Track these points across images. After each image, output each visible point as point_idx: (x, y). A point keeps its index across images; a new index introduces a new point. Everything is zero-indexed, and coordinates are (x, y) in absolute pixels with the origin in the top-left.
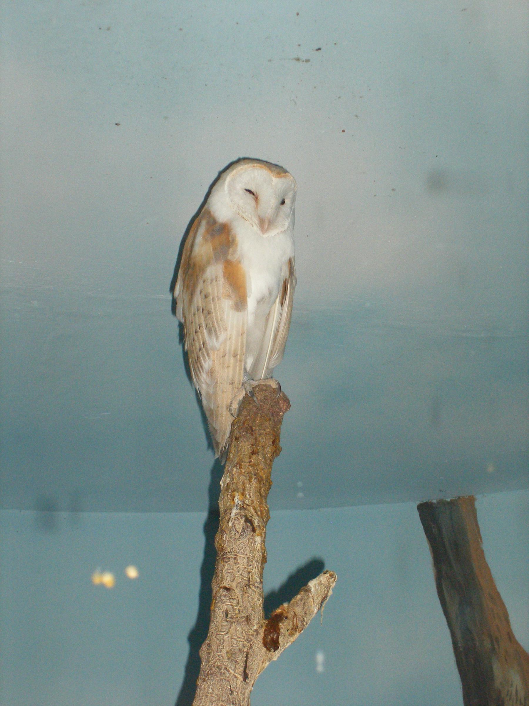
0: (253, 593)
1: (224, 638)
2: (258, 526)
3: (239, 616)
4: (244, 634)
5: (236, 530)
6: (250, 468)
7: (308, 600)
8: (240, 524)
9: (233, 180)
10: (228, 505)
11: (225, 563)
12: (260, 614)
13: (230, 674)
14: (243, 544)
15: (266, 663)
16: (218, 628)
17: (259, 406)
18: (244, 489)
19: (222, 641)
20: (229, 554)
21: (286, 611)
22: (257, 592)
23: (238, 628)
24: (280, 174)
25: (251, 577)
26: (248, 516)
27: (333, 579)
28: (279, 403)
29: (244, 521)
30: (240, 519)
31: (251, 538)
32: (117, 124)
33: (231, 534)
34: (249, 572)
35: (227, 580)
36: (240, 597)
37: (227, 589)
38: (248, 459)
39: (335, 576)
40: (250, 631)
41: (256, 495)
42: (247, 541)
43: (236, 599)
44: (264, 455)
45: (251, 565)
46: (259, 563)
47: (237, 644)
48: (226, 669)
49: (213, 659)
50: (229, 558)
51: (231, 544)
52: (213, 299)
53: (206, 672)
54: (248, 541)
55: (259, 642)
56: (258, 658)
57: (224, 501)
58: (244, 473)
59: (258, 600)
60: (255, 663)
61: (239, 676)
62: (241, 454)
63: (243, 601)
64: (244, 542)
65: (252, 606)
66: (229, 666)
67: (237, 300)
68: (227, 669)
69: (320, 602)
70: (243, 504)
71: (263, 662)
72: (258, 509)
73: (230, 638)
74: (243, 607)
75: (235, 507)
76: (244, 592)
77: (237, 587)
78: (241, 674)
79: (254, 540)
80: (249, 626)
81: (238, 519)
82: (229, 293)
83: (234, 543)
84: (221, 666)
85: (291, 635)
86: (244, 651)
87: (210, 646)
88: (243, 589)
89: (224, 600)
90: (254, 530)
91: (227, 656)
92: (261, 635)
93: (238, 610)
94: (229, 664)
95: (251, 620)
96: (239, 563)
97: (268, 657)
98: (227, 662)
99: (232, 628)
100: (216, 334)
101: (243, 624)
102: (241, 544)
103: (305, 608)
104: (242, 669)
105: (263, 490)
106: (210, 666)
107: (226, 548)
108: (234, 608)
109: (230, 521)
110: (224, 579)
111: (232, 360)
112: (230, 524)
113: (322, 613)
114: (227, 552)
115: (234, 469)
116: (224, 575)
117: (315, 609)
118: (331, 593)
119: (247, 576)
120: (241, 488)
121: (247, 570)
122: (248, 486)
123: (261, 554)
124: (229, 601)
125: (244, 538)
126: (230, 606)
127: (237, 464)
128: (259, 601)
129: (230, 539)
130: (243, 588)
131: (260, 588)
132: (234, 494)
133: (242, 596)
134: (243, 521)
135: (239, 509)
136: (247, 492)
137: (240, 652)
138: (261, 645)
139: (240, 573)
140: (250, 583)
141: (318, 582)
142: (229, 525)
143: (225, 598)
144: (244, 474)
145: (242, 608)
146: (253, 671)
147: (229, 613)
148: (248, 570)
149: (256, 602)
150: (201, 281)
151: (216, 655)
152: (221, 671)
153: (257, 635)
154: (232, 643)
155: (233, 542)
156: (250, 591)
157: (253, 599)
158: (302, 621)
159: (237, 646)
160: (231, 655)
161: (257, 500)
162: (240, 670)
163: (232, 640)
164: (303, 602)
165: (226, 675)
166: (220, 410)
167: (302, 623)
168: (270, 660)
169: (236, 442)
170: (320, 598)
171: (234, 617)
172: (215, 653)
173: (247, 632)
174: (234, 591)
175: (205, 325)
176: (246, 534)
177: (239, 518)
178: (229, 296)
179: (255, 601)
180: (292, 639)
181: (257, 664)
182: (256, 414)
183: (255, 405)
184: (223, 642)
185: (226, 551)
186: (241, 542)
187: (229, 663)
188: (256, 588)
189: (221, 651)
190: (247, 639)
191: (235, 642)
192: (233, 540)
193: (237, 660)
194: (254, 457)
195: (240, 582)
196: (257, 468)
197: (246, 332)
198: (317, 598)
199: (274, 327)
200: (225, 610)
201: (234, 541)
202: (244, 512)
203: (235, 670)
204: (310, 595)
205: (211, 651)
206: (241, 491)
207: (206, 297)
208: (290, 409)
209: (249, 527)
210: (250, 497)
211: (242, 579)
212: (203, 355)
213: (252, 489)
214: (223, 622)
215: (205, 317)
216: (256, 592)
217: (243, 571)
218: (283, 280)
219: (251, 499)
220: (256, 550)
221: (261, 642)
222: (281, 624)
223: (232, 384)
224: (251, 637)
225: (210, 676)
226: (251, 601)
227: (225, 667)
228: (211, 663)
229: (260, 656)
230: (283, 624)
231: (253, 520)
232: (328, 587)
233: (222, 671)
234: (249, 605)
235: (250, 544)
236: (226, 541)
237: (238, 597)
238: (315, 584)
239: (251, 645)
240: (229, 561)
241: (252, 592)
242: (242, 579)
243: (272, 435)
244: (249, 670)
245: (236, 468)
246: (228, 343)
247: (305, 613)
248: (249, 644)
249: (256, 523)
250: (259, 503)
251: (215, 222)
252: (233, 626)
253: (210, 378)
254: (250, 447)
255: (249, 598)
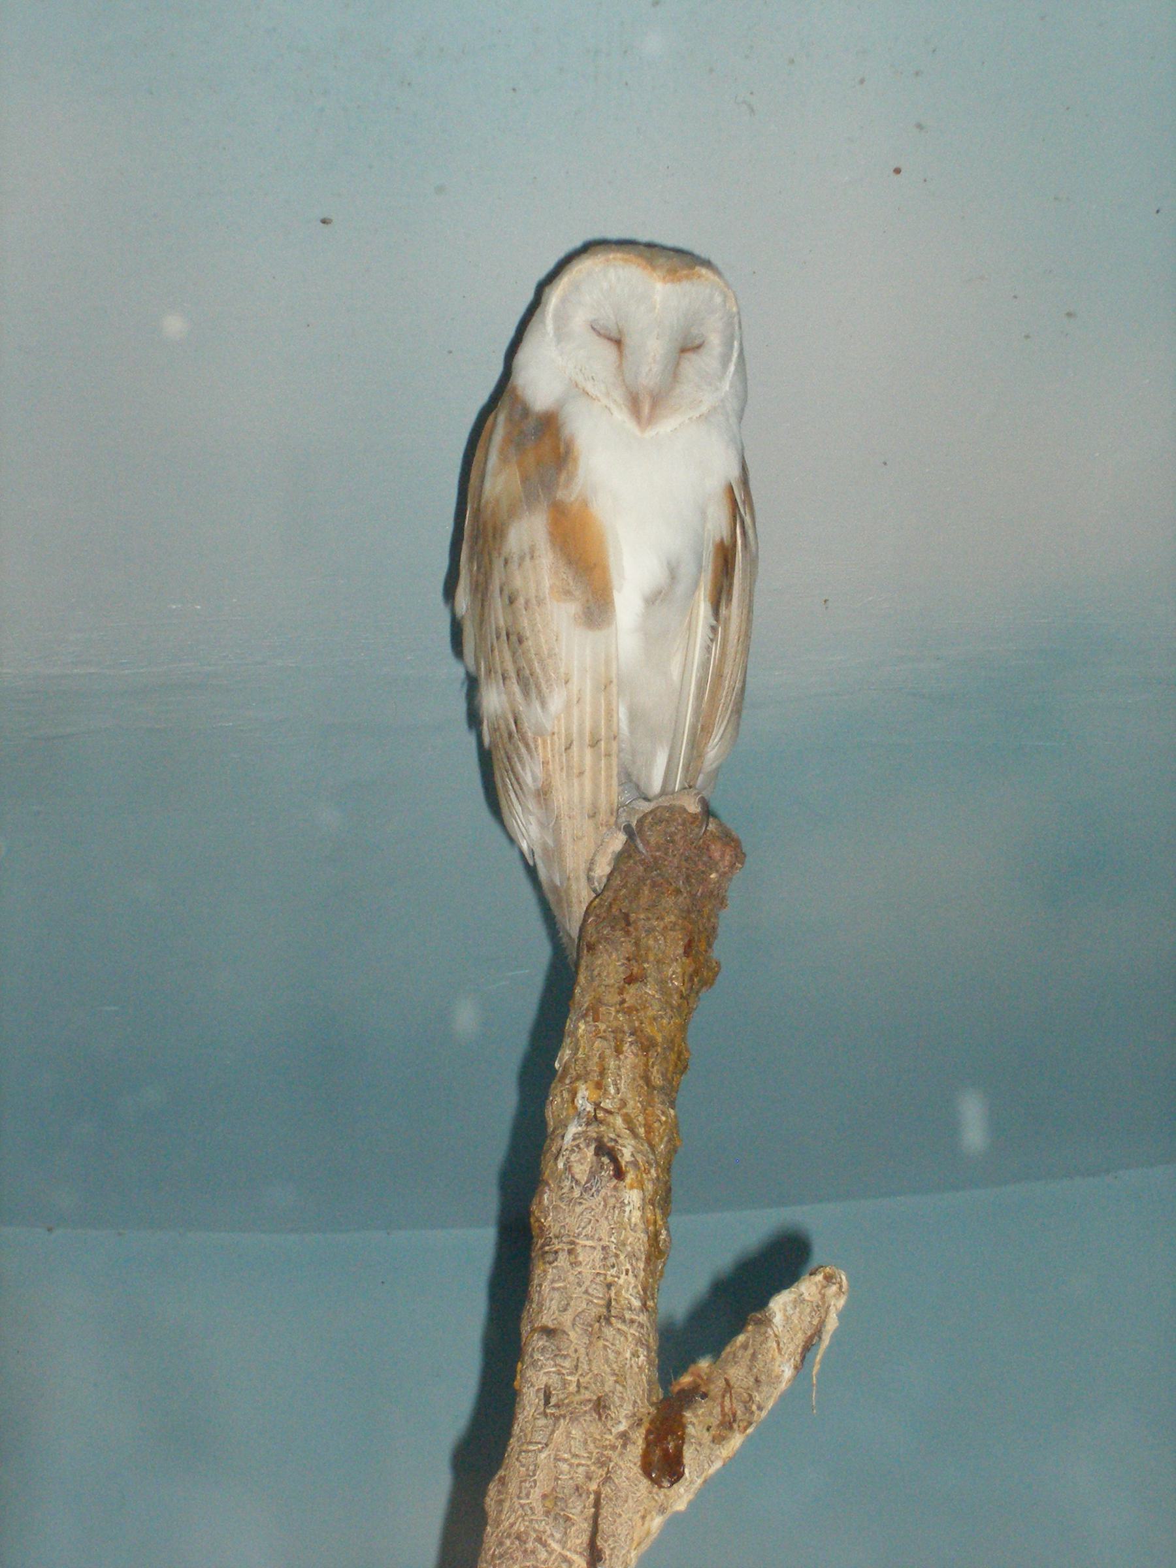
0: (618, 1336)
1: (536, 1459)
2: (632, 1161)
3: (577, 1398)
4: (591, 1446)
5: (573, 1177)
6: (621, 1019)
7: (764, 1346)
8: (583, 1162)
9: (564, 300)
10: (562, 1117)
11: (548, 1266)
12: (641, 1392)
13: (550, 1553)
14: (590, 1213)
15: (652, 1519)
16: (525, 1435)
17: (652, 860)
18: (602, 1073)
19: (531, 1468)
20: (555, 1241)
21: (705, 1378)
22: (631, 1333)
23: (573, 1432)
24: (676, 271)
25: (613, 1295)
26: (606, 1140)
27: (834, 1288)
28: (708, 850)
29: (593, 1152)
30: (585, 1149)
31: (612, 1196)
32: (324, 221)
33: (562, 1188)
34: (609, 1286)
35: (549, 1308)
36: (582, 1351)
37: (549, 1332)
38: (616, 995)
39: (839, 1280)
40: (607, 1436)
41: (636, 1084)
42: (600, 1204)
43: (570, 1357)
44: (662, 983)
45: (613, 1266)
46: (637, 1259)
47: (572, 1473)
48: (539, 1540)
49: (509, 1517)
50: (556, 1252)
51: (561, 1216)
52: (527, 602)
53: (491, 1552)
54: (602, 1203)
55: (632, 1465)
56: (629, 1506)
57: (554, 1108)
58: (604, 1032)
59: (635, 1354)
60: (623, 1522)
61: (575, 1557)
62: (599, 986)
63: (590, 1360)
64: (594, 1207)
65: (616, 1371)
66: (549, 1532)
67: (588, 601)
68: (543, 1539)
69: (800, 1350)
70: (595, 1110)
71: (643, 1517)
72: (638, 1120)
73: (552, 1460)
74: (589, 1376)
75: (576, 1120)
76: (594, 1335)
77: (573, 1325)
78: (581, 1553)
79: (620, 1201)
80: (605, 1425)
81: (580, 1148)
82: (569, 584)
83: (569, 1212)
84: (527, 1534)
85: (718, 1440)
86: (588, 1490)
87: (503, 1484)
88: (590, 1329)
89: (540, 1360)
90: (619, 1174)
91: (544, 1506)
92: (638, 1446)
93: (575, 1384)
94: (547, 1528)
95: (612, 1407)
96: (581, 1263)
97: (656, 1501)
98: (543, 1523)
99: (557, 1432)
100: (539, 691)
101: (585, 1420)
102: (585, 1213)
103: (756, 1367)
104: (585, 1538)
105: (655, 1071)
106: (500, 1534)
107: (550, 1226)
108: (564, 1379)
109: (561, 1157)
110: (544, 1308)
111: (588, 753)
112: (561, 1165)
113: (814, 1379)
114: (553, 1237)
115: (580, 1024)
116: (545, 1296)
117: (787, 1370)
118: (832, 1323)
119: (601, 1296)
120: (595, 1071)
121: (602, 1279)
122: (612, 1064)
123: (642, 1235)
124: (552, 1363)
125: (593, 1196)
126: (554, 1375)
127: (587, 1010)
128: (638, 1357)
129: (559, 1203)
130: (591, 1326)
131: (639, 1323)
132: (576, 1087)
133: (587, 1348)
134: (590, 1152)
135: (584, 1124)
136: (609, 1080)
137: (577, 1494)
138: (636, 1471)
139: (583, 1289)
140: (610, 1311)
141: (793, 1296)
142: (557, 1167)
143: (542, 1356)
144: (604, 1034)
145: (587, 1378)
146: (616, 1542)
147: (553, 1392)
148: (605, 1279)
149: (628, 1362)
150: (498, 564)
151: (517, 1506)
152: (527, 1546)
153: (624, 1446)
154: (557, 1472)
155: (565, 1210)
156: (609, 1332)
157: (618, 1353)
158: (745, 1402)
159: (572, 1478)
160: (553, 1503)
161: (637, 1098)
162: (578, 1541)
163: (559, 1463)
164: (750, 1351)
165: (539, 1557)
166: (574, 887)
167: (745, 1407)
168: (662, 1510)
169: (589, 957)
170: (800, 1339)
171: (563, 1404)
172: (515, 1499)
173: (599, 1440)
174: (566, 1337)
175: (516, 674)
176: (598, 1184)
177: (582, 1146)
178: (568, 593)
179: (627, 1359)
180: (722, 1450)
181: (626, 1522)
182: (641, 880)
183: (643, 860)
184: (534, 1471)
185: (549, 1234)
186: (584, 1207)
187: (547, 1524)
188: (626, 1325)
189: (528, 1495)
190: (598, 1459)
191: (564, 1467)
192: (565, 1205)
193: (571, 1515)
194: (632, 989)
195: (583, 1311)
196: (638, 1017)
197: (615, 681)
198: (790, 1340)
199: (698, 663)
200: (543, 1387)
201: (569, 1205)
202: (596, 1130)
203: (566, 1542)
204: (770, 1331)
205: (505, 1495)
206: (596, 1079)
207: (512, 601)
208: (743, 864)
209: (605, 1167)
210: (618, 1091)
211: (589, 1302)
212: (517, 749)
213: (623, 1070)
214: (538, 1419)
215: (514, 654)
216: (629, 1335)
217: (592, 1281)
218: (714, 541)
219: (619, 1095)
220: (629, 1227)
221: (635, 1464)
222: (688, 1414)
223: (593, 816)
224: (609, 1453)
225: (498, 1562)
226: (615, 1360)
227: (537, 1536)
228: (503, 1526)
229: (635, 1500)
230: (694, 1414)
231: (620, 1148)
232: (821, 1308)
233: (530, 1545)
234: (608, 1370)
235: (609, 1211)
236: (551, 1207)
237: (576, 1351)
238: (785, 1304)
239: (608, 1472)
240: (556, 1259)
241: (614, 1335)
242: (587, 1304)
243: (682, 929)
244: (606, 1541)
245: (586, 1022)
246: (575, 711)
247: (757, 1381)
248: (603, 1471)
249: (626, 1154)
250: (642, 1106)
251: (526, 412)
252: (561, 1428)
253: (544, 807)
254: (623, 964)
255: (606, 1350)
